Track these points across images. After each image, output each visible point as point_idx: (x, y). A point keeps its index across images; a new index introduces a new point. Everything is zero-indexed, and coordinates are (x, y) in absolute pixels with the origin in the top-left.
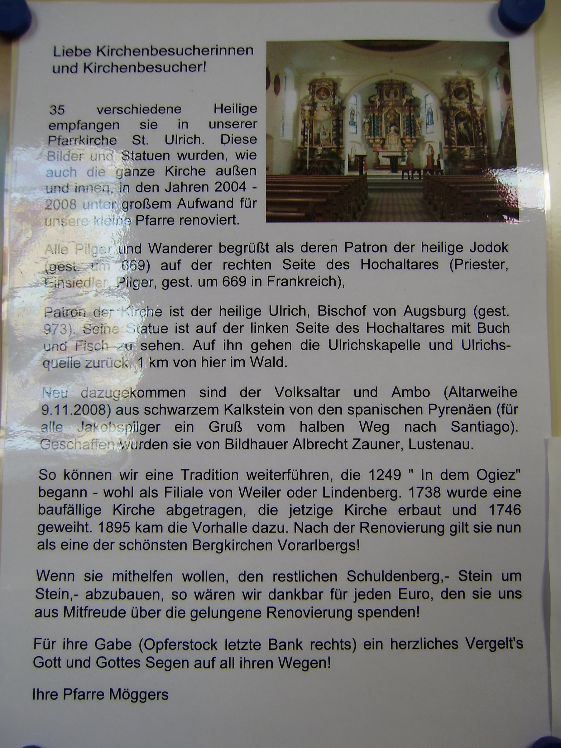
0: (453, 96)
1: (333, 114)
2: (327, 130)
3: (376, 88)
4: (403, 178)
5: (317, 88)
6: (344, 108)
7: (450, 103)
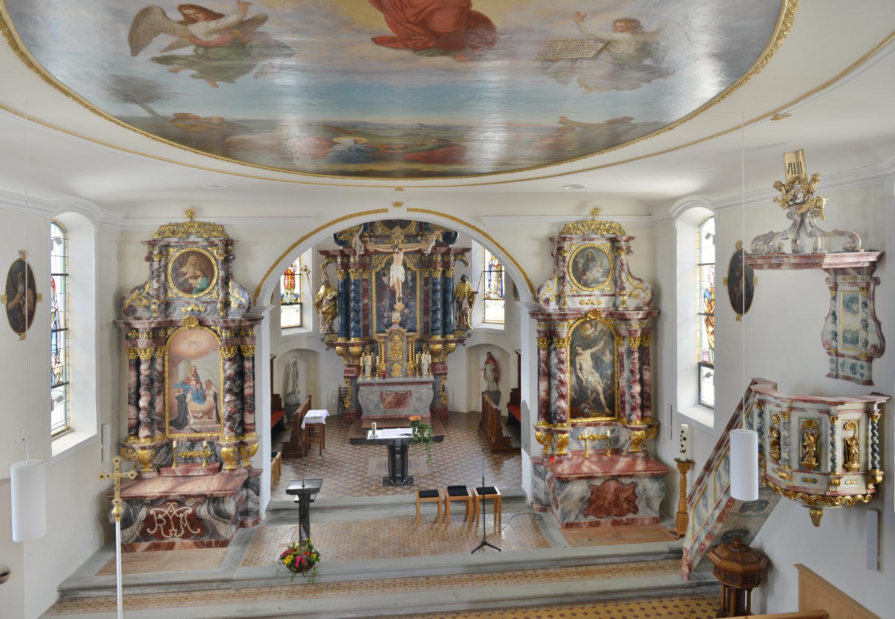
0: (570, 277)
1: (228, 343)
2: (209, 383)
4: (53, 331)
5: (174, 254)
6: (255, 320)
7: (559, 297)
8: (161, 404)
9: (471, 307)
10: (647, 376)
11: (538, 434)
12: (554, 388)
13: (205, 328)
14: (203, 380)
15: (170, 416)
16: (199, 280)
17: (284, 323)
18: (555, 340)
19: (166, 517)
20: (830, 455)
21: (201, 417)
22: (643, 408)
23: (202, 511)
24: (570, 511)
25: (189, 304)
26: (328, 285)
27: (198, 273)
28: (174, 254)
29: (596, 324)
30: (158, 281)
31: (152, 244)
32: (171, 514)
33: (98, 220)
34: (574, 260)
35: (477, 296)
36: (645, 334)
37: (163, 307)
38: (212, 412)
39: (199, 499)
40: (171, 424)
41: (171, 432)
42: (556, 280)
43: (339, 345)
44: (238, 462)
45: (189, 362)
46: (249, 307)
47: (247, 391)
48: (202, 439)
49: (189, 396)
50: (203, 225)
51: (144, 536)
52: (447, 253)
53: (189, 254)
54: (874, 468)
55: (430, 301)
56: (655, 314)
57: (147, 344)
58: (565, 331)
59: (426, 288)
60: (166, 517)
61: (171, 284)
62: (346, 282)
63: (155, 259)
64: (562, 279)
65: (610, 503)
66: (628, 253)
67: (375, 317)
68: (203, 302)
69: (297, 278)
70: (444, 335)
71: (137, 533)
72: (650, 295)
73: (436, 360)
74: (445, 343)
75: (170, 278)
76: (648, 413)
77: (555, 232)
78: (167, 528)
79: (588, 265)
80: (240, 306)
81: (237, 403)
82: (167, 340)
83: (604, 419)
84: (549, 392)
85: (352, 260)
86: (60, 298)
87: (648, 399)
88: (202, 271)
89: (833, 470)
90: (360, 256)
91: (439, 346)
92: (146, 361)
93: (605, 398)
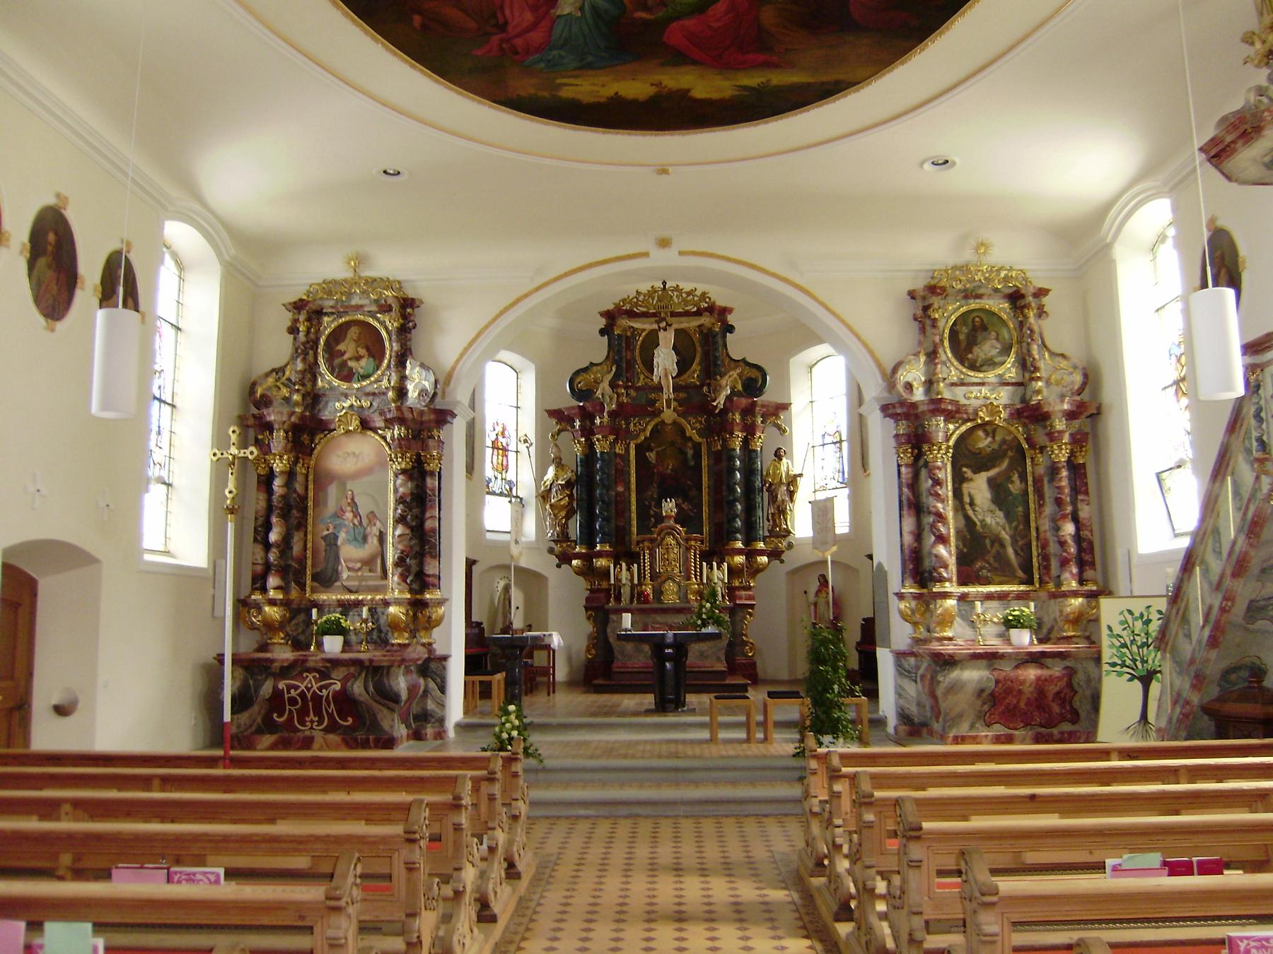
0: (946, 353)
1: (402, 445)
2: (372, 516)
3: (602, 332)
5: (329, 324)
6: (443, 417)
7: (929, 384)
8: (301, 544)
9: (792, 500)
10: (1085, 512)
11: (902, 605)
12: (927, 528)
13: (370, 433)
14: (363, 511)
15: (313, 566)
16: (363, 362)
18: (926, 447)
19: (302, 695)
21: (359, 569)
22: (1082, 564)
23: (355, 687)
24: (960, 716)
25: (346, 396)
26: (559, 464)
27: (362, 351)
28: (329, 324)
29: (994, 432)
30: (304, 360)
31: (298, 306)
32: (308, 689)
33: (227, 257)
34: (952, 330)
36: (1079, 440)
37: (309, 400)
38: (375, 562)
39: (352, 669)
40: (314, 578)
41: (313, 591)
42: (923, 359)
43: (577, 556)
44: (413, 634)
45: (344, 484)
46: (435, 394)
47: (429, 524)
48: (359, 604)
49: (342, 536)
50: (372, 282)
51: (268, 726)
52: (749, 411)
53: (348, 325)
55: (724, 487)
56: (1091, 412)
58: (944, 432)
60: (302, 695)
61: (323, 368)
62: (589, 457)
64: (932, 355)
65: (1028, 703)
66: (1040, 316)
67: (634, 515)
68: (368, 394)
69: (512, 456)
70: (749, 540)
71: (259, 720)
73: (737, 583)
74: (751, 554)
75: (321, 360)
76: (1089, 573)
77: (919, 284)
78: (303, 713)
80: (423, 392)
81: (413, 542)
82: (313, 449)
83: (1014, 588)
84: (918, 536)
85: (598, 421)
87: (1091, 550)
88: (368, 349)
90: (611, 414)
91: (739, 559)
92: (282, 472)
93: (1016, 553)
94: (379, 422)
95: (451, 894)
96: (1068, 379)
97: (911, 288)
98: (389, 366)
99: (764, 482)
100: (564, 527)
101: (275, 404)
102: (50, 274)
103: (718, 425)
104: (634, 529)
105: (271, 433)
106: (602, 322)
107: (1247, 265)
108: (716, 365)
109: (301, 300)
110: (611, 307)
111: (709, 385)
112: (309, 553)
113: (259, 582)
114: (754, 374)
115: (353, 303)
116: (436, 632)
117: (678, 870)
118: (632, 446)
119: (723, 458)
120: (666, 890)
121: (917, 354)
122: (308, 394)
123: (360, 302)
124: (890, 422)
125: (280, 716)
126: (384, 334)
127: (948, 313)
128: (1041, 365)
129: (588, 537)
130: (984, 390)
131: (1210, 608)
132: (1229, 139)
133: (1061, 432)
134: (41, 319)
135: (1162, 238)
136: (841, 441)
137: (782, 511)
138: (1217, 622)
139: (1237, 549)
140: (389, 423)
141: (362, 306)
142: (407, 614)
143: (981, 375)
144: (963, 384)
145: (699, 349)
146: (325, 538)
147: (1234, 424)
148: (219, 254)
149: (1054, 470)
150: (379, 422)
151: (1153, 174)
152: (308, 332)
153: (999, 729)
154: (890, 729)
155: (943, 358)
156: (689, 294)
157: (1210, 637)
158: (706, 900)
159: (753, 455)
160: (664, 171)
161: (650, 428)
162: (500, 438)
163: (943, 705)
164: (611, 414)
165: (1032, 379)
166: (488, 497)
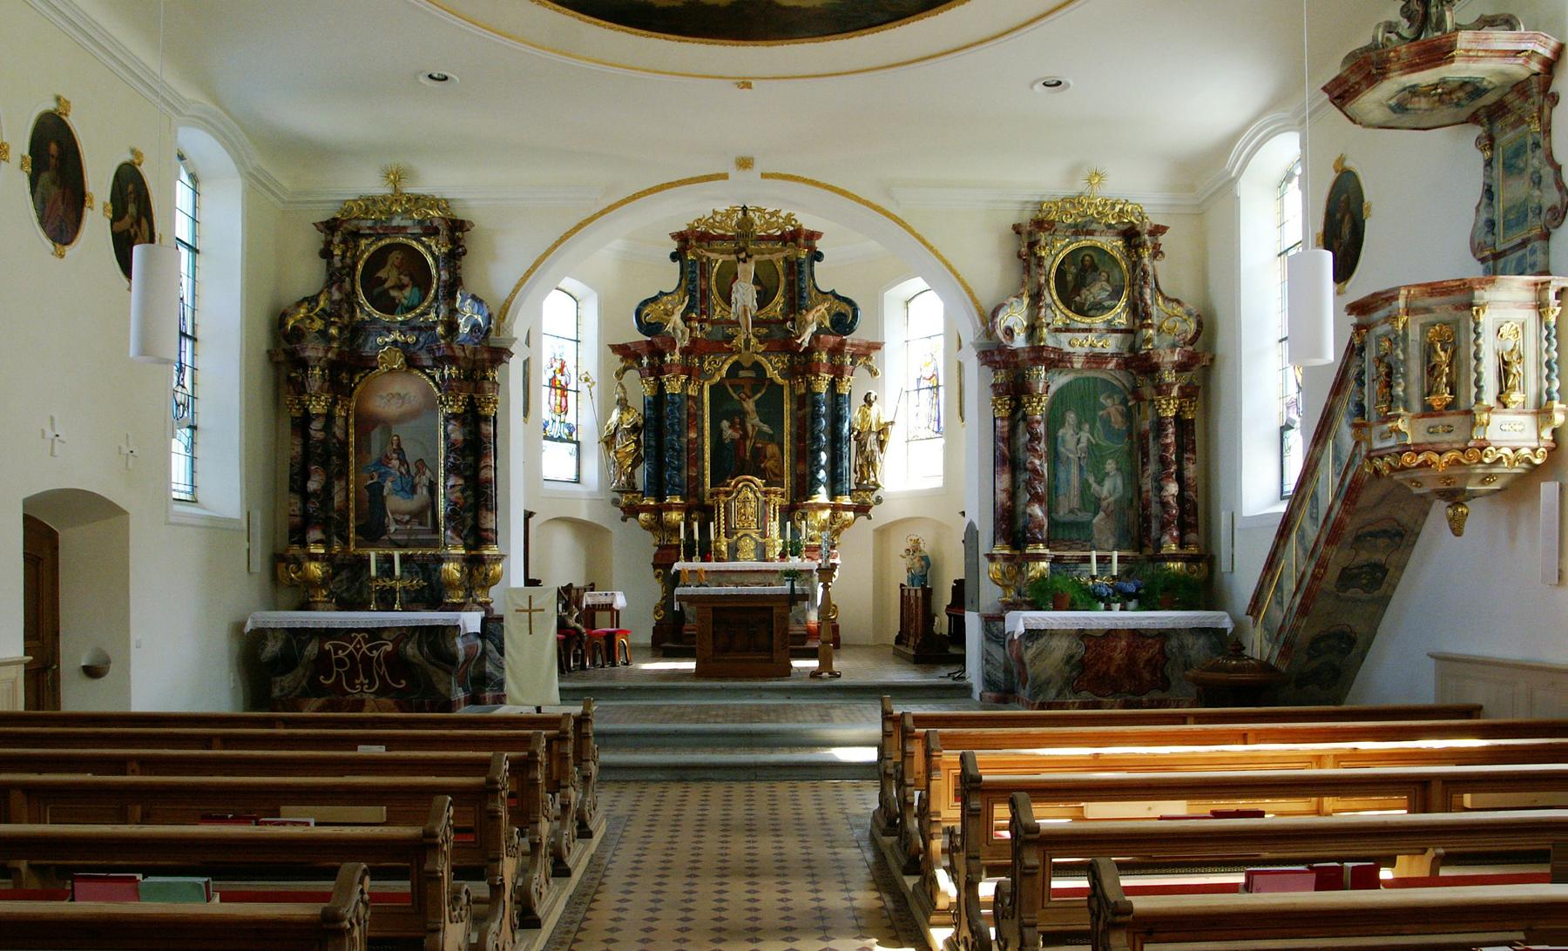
0: (1051, 296)
2: (421, 464)
3: (674, 257)
5: (367, 248)
6: (499, 355)
7: (1032, 330)
8: (343, 494)
10: (1191, 471)
11: (994, 567)
13: (416, 372)
16: (407, 292)
17: (548, 472)
19: (351, 656)
20: (1474, 376)
22: (1184, 527)
25: (389, 331)
26: (623, 405)
27: (406, 280)
30: (340, 289)
31: (330, 226)
32: (358, 650)
35: (893, 430)
36: (1188, 393)
37: (347, 334)
42: (1026, 300)
43: (646, 509)
49: (388, 485)
50: (417, 200)
52: (836, 351)
54: (1550, 399)
56: (1204, 362)
57: (321, 388)
59: (801, 413)
62: (658, 401)
63: (337, 252)
64: (1036, 298)
67: (707, 465)
69: (571, 396)
70: (833, 495)
71: (304, 683)
72: (1193, 326)
76: (1192, 537)
77: (1026, 217)
78: (352, 676)
79: (1084, 278)
80: (475, 327)
84: (1013, 494)
85: (668, 358)
86: (186, 282)
88: (412, 278)
89: (1478, 399)
94: (427, 360)
95: (528, 848)
96: (1185, 327)
97: (1016, 222)
98: (436, 298)
99: (851, 429)
100: (631, 476)
101: (309, 337)
102: (55, 191)
103: (802, 364)
104: (708, 480)
105: (306, 370)
106: (674, 246)
107: (1373, 212)
108: (802, 297)
109: (335, 219)
110: (684, 228)
111: (793, 320)
112: (352, 505)
113: (298, 534)
114: (844, 308)
115: (394, 223)
116: (494, 591)
117: (750, 829)
118: (707, 387)
119: (807, 401)
120: (738, 846)
121: (1019, 296)
122: (346, 327)
123: (404, 223)
124: (987, 370)
125: (328, 677)
126: (430, 260)
127: (1055, 252)
128: (1154, 310)
129: (658, 486)
130: (1091, 337)
131: (1303, 575)
132: (1353, 79)
133: (1170, 385)
134: (49, 243)
135: (1288, 177)
136: (938, 387)
137: (870, 463)
138: (1309, 589)
139: (1333, 515)
140: (439, 362)
141: (405, 228)
142: (462, 571)
143: (1088, 320)
144: (1067, 330)
145: (783, 279)
146: (368, 487)
147: (1338, 388)
148: (239, 161)
149: (1160, 425)
150: (427, 360)
151: (1278, 109)
152: (343, 256)
153: (1086, 695)
154: (976, 696)
155: (1048, 300)
156: (772, 215)
157: (1301, 604)
158: (783, 904)
159: (841, 400)
160: (749, 86)
161: (726, 367)
162: (559, 376)
163: (1030, 671)
164: (684, 351)
165: (1143, 326)
166: (546, 443)
